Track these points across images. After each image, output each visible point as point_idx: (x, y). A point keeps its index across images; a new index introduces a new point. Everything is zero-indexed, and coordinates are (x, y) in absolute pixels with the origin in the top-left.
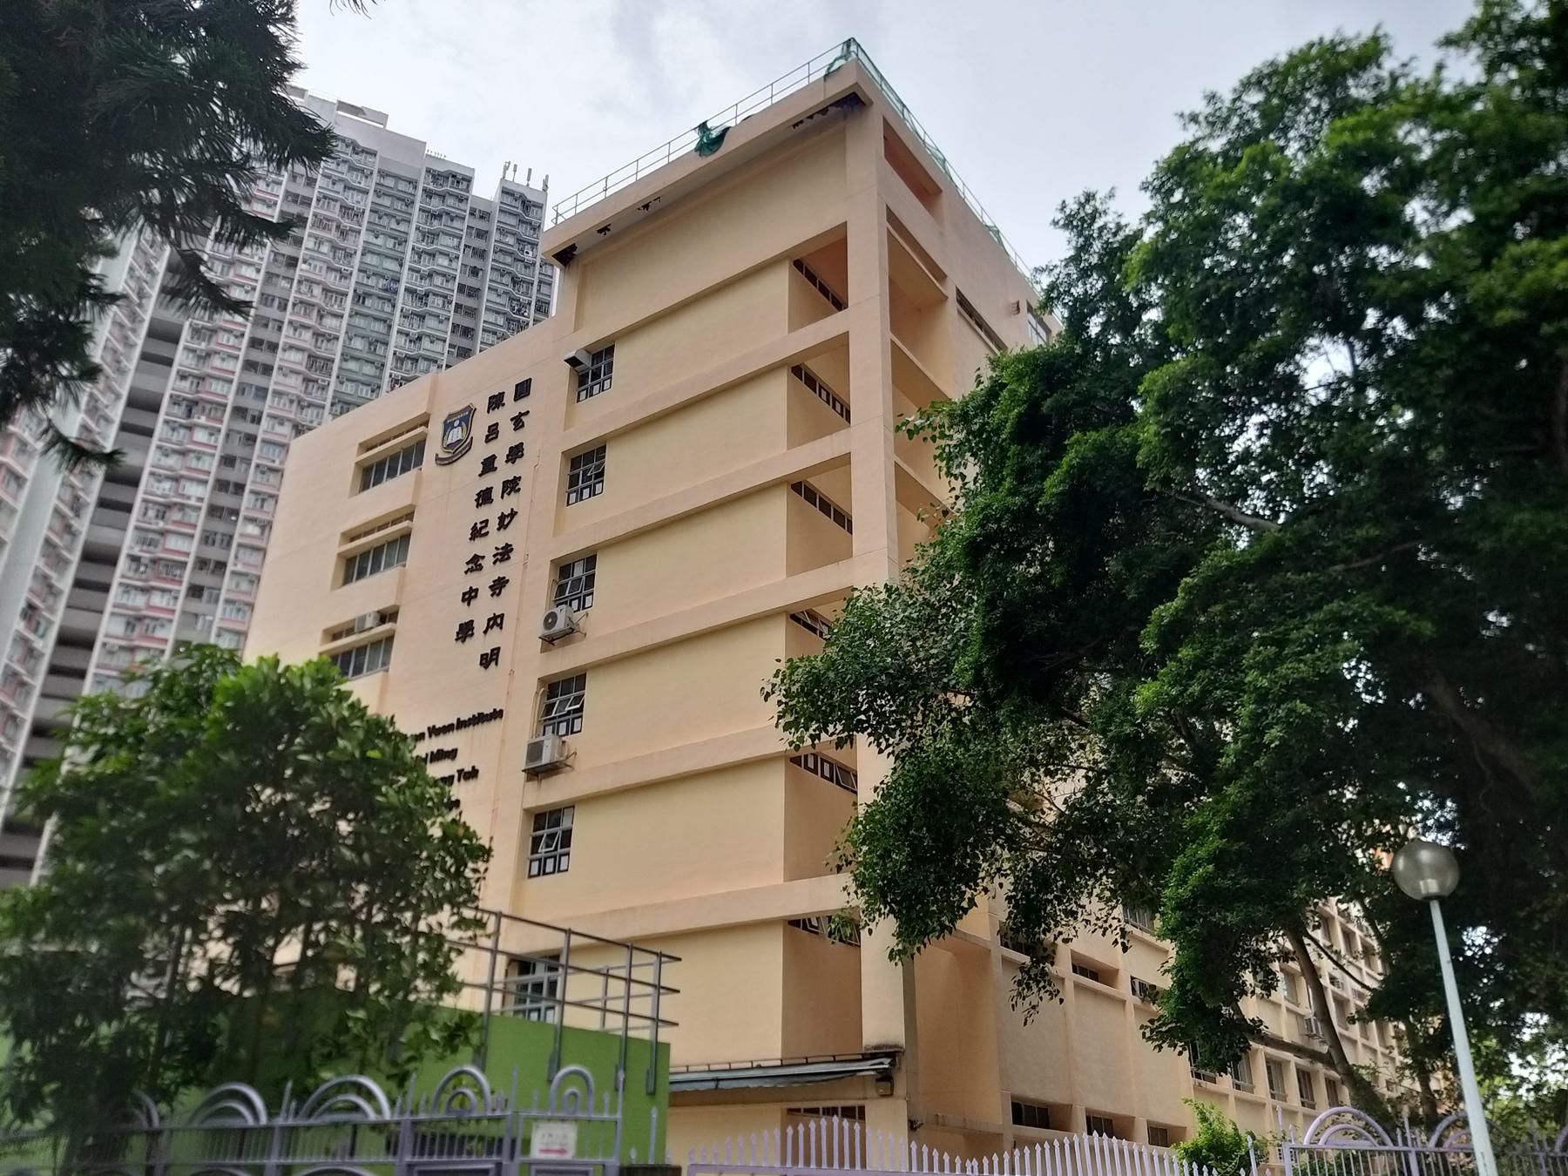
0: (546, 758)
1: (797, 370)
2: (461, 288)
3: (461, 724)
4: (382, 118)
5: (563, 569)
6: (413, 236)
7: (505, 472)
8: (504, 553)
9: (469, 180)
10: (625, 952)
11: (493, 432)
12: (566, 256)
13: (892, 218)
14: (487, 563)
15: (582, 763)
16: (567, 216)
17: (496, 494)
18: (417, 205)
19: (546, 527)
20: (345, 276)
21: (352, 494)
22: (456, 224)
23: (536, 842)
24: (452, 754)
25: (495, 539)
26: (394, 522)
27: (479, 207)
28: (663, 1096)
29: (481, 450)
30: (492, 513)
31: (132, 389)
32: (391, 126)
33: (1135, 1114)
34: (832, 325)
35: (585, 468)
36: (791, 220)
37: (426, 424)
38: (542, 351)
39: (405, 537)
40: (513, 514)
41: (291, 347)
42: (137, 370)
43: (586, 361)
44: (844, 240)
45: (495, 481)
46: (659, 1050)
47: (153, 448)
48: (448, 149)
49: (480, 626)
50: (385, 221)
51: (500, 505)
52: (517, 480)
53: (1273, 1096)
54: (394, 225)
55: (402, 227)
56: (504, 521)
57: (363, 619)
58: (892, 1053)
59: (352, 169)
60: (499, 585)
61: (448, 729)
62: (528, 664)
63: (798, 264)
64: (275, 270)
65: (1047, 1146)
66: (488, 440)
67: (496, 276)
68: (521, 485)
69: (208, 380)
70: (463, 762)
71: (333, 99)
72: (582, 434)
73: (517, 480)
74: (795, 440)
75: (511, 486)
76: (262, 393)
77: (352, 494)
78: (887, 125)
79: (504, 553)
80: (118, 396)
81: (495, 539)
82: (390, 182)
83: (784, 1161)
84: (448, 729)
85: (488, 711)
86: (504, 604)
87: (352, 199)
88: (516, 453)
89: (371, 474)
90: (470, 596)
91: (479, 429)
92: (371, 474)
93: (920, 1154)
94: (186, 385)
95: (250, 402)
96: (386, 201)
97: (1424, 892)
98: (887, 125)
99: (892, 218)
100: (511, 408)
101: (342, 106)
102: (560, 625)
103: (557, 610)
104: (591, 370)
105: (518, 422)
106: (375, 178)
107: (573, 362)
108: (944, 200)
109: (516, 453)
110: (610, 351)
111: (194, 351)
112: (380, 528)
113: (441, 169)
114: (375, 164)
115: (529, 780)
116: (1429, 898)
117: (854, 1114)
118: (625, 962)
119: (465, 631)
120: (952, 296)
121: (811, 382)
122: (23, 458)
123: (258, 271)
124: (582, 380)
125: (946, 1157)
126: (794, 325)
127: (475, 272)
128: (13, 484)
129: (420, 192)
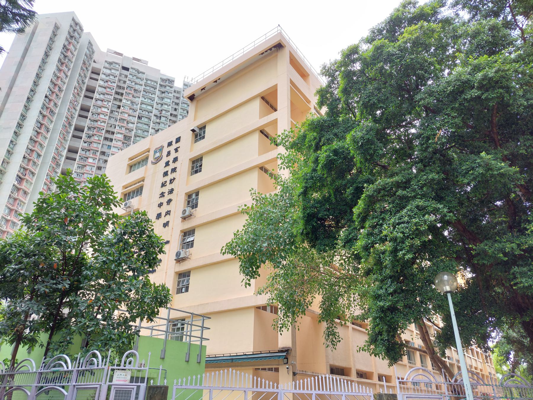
1: (262, 132)
2: (171, 115)
4: (146, 63)
5: (189, 196)
6: (156, 99)
7: (172, 166)
8: (171, 191)
9: (174, 81)
10: (201, 318)
11: (169, 154)
12: (192, 98)
13: (292, 82)
14: (166, 194)
15: (193, 257)
17: (169, 173)
18: (158, 89)
19: (184, 183)
20: (135, 111)
21: (126, 174)
22: (170, 95)
23: (179, 282)
25: (169, 187)
26: (139, 182)
27: (177, 90)
28: (203, 363)
29: (165, 159)
30: (168, 179)
31: (69, 146)
32: (149, 65)
33: (374, 371)
34: (273, 116)
35: (196, 165)
36: (259, 85)
37: (149, 152)
38: (183, 128)
39: (141, 188)
40: (174, 179)
41: (119, 133)
42: (71, 140)
43: (197, 130)
44: (276, 90)
45: (169, 169)
46: (202, 348)
47: (76, 164)
48: (168, 73)
49: (163, 214)
50: (147, 94)
51: (170, 176)
52: (175, 168)
53: (433, 369)
54: (150, 95)
55: (153, 96)
56: (172, 181)
58: (287, 351)
59: (137, 78)
60: (169, 202)
63: (263, 98)
64: (113, 109)
65: (316, 378)
66: (167, 156)
67: (182, 111)
68: (177, 170)
69: (93, 143)
71: (131, 56)
72: (195, 154)
73: (175, 168)
74: (261, 153)
75: (174, 170)
76: (109, 147)
77: (126, 174)
79: (171, 191)
80: (65, 148)
81: (169, 187)
82: (149, 82)
83: (253, 387)
87: (137, 87)
88: (175, 160)
89: (131, 167)
90: (160, 205)
91: (165, 153)
92: (131, 167)
93: (253, 379)
94: (86, 145)
95: (105, 149)
96: (148, 88)
97: (445, 291)
99: (292, 82)
100: (174, 146)
101: (134, 59)
102: (187, 213)
103: (186, 209)
104: (199, 134)
105: (176, 150)
106: (145, 81)
107: (193, 131)
108: (310, 77)
109: (175, 160)
110: (205, 127)
112: (134, 184)
113: (165, 78)
115: (176, 263)
116: (447, 292)
117: (277, 370)
118: (201, 322)
122: (34, 167)
124: (196, 136)
125: (271, 383)
126: (261, 117)
127: (176, 110)
128: (31, 175)
129: (158, 85)
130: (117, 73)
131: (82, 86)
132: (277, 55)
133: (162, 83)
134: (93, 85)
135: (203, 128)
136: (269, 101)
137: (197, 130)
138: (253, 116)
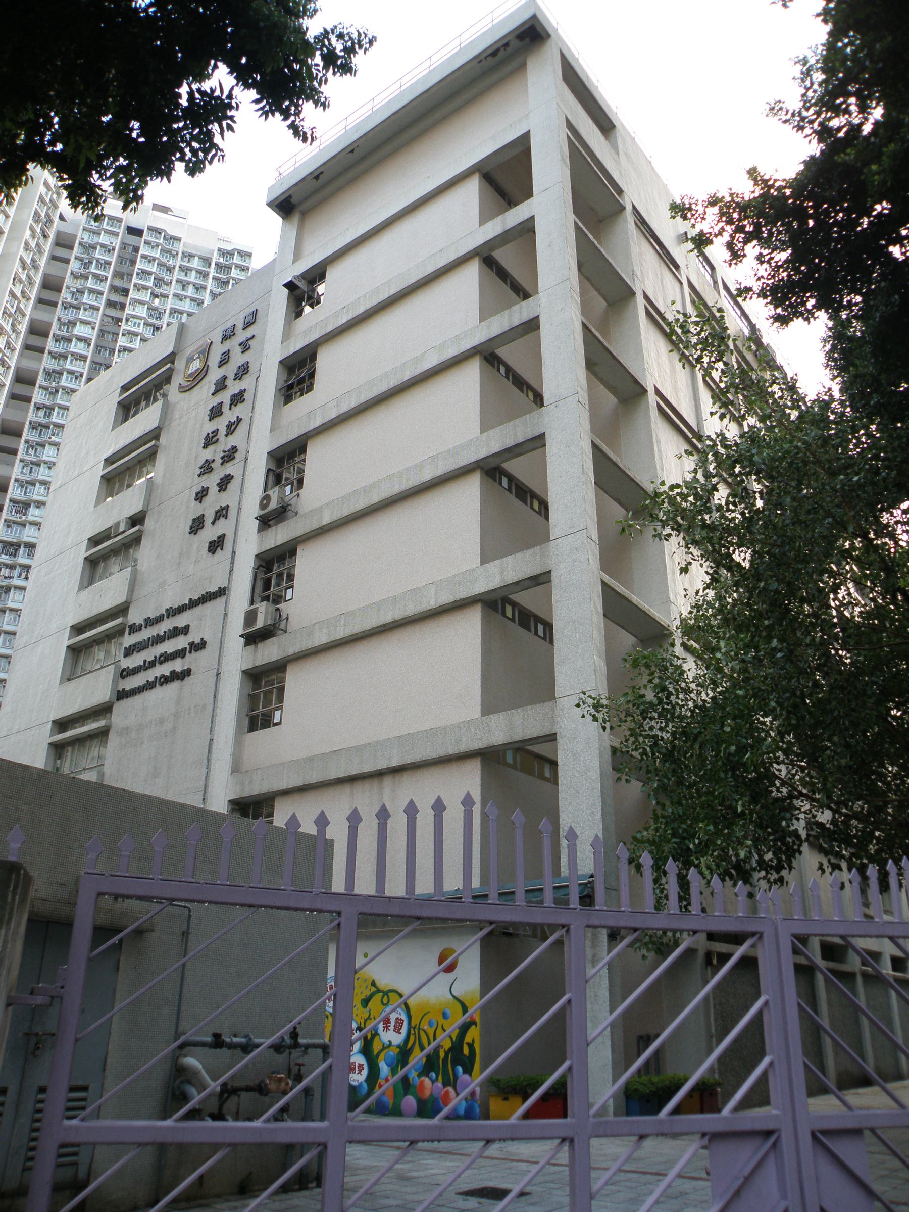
0: (260, 623)
3: (193, 604)
9: (249, 255)
13: (570, 125)
16: (285, 174)
24: (185, 630)
29: (215, 374)
35: (298, 374)
36: (478, 138)
40: (239, 420)
47: (18, 460)
52: (242, 392)
57: (117, 525)
61: (181, 609)
62: (249, 543)
70: (194, 636)
78: (563, 56)
84: (181, 609)
85: (214, 589)
86: (228, 498)
89: (127, 409)
90: (201, 495)
91: (215, 358)
92: (127, 409)
98: (563, 56)
99: (570, 125)
102: (273, 505)
111: (46, 389)
113: (229, 248)
114: (180, 248)
119: (197, 525)
120: (629, 208)
121: (502, 274)
123: (93, 328)
130: (117, 243)
131: (32, 273)
132: (523, 66)
133: (221, 260)
134: (58, 274)
135: (317, 275)
136: (505, 177)
137: (302, 285)
138: (462, 223)
